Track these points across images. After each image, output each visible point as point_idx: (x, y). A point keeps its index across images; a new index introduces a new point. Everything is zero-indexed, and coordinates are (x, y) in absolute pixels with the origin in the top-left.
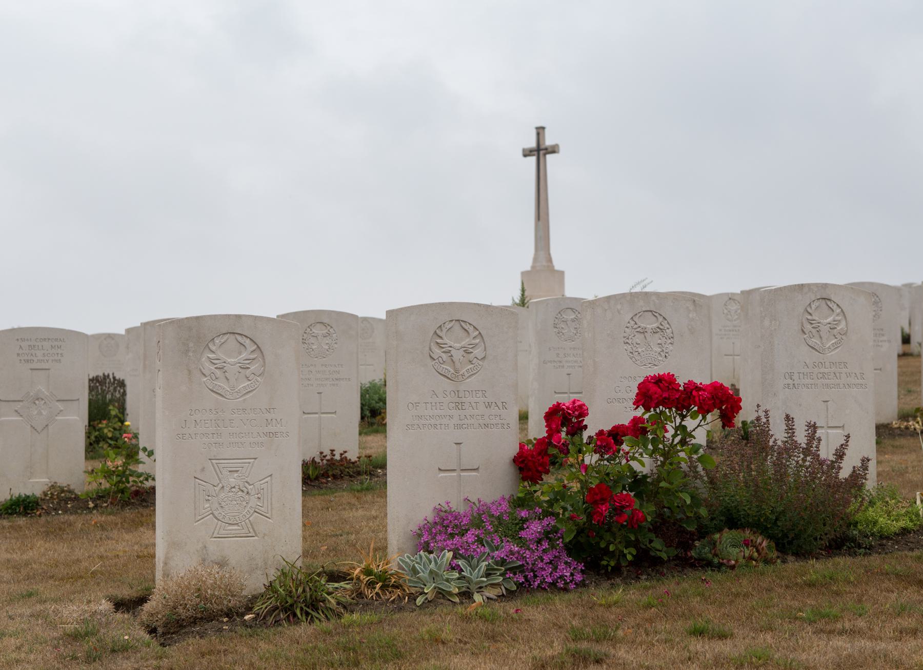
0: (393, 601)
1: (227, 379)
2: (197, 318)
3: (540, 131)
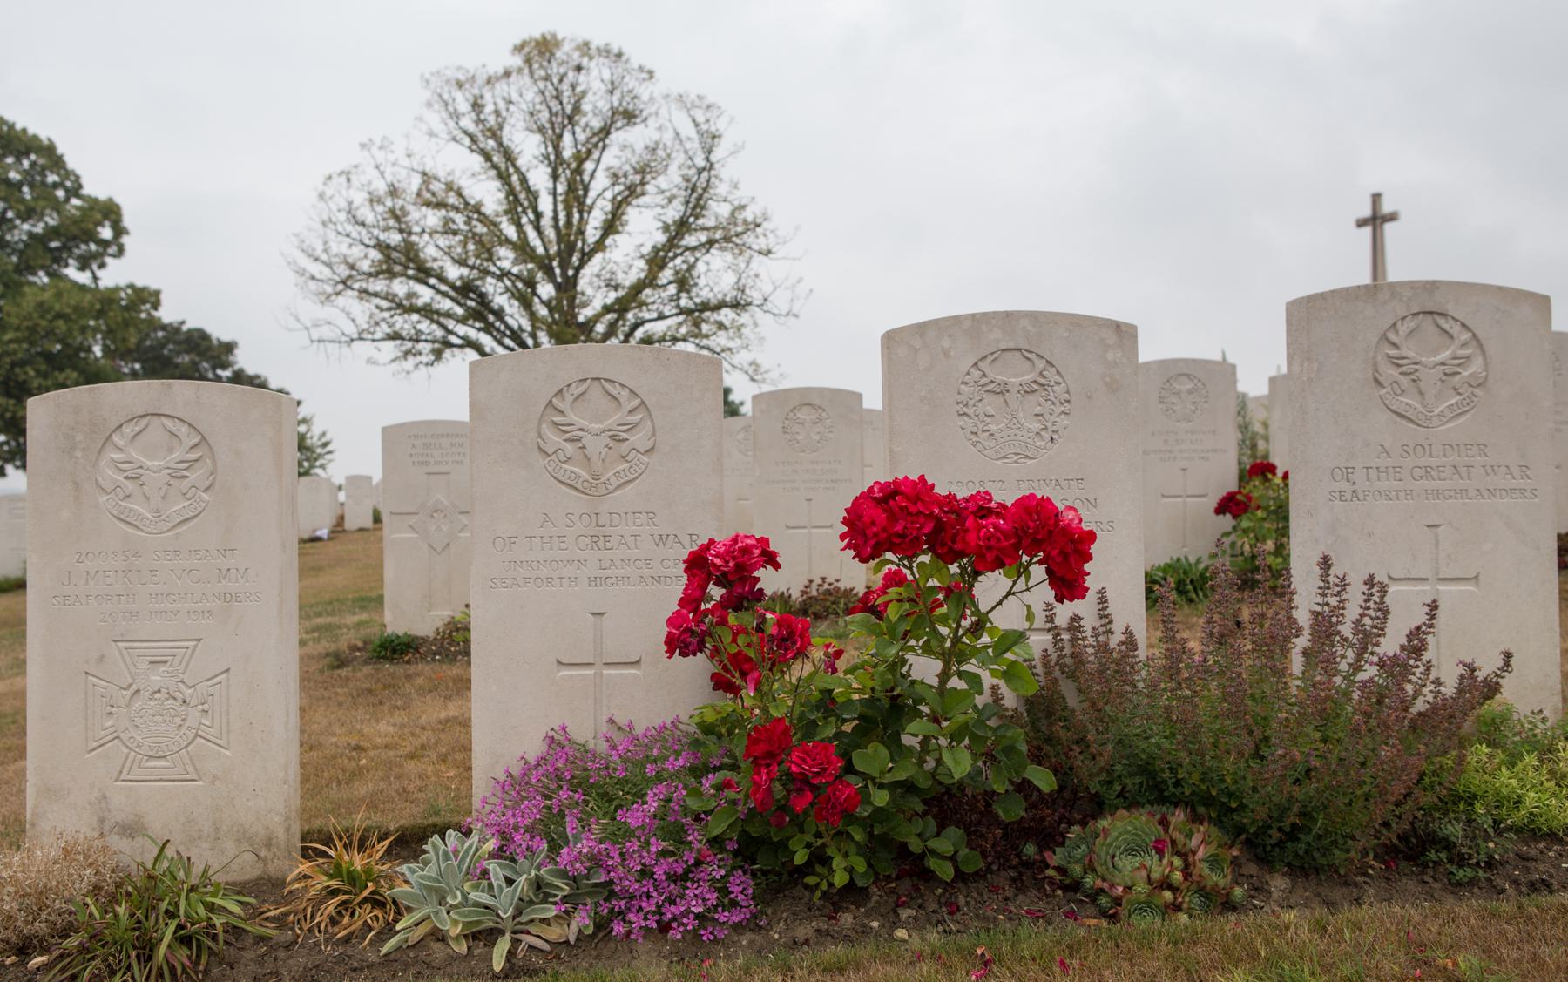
1: (148, 498)
3: (1376, 198)
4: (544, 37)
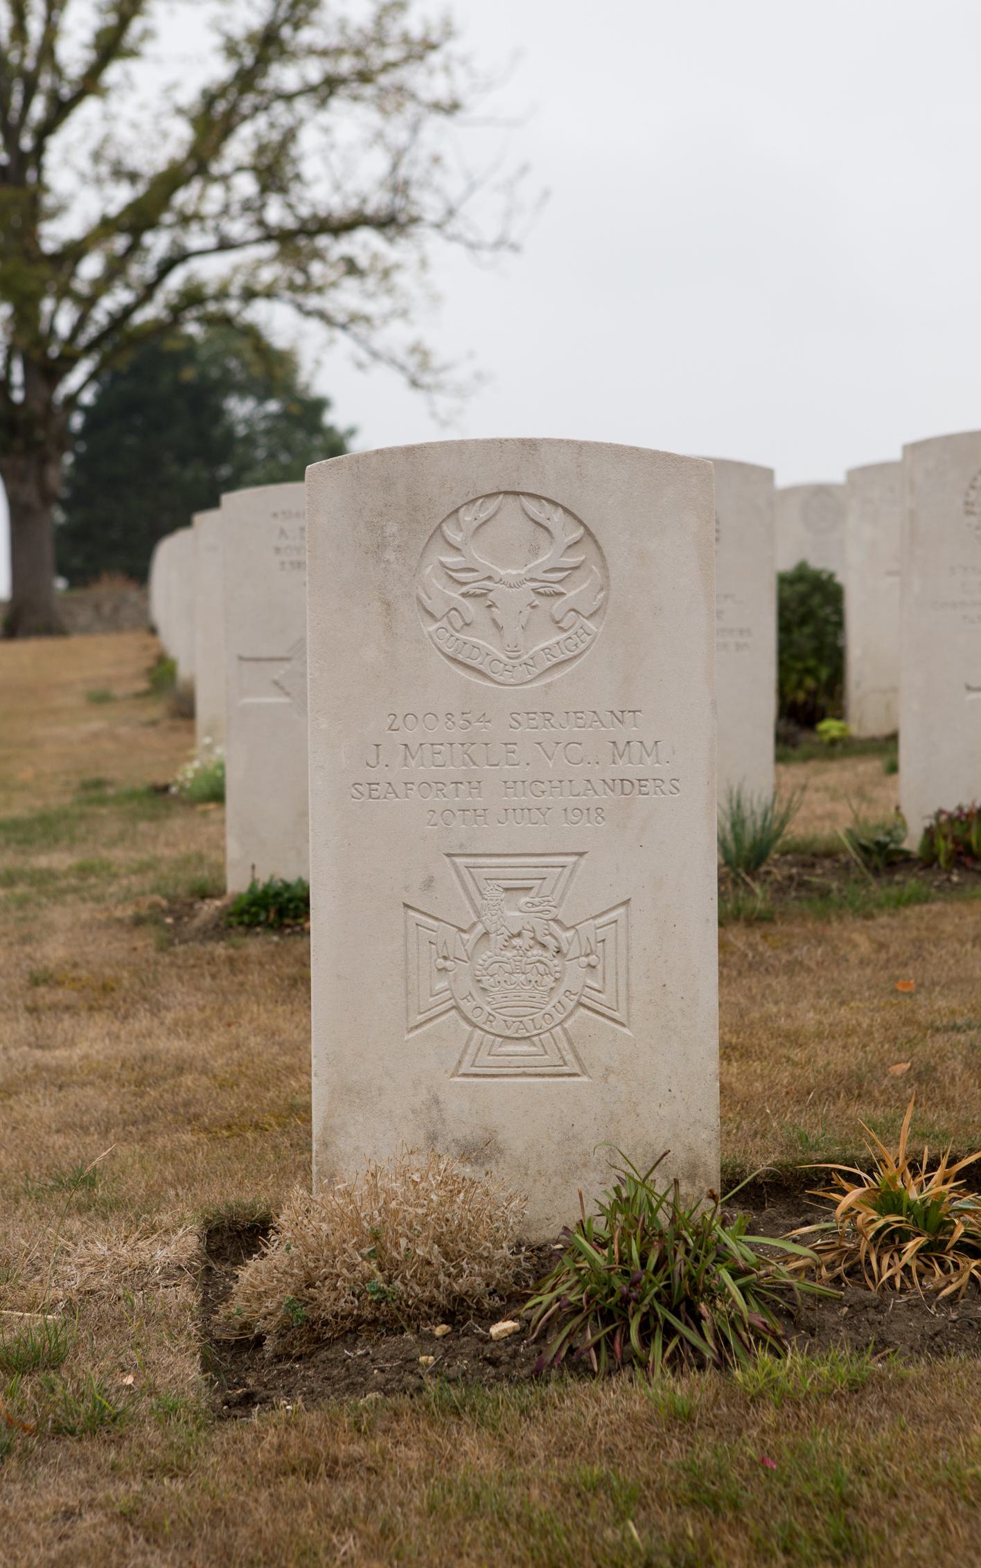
0: (952, 1300)
1: (499, 628)
2: (410, 451)
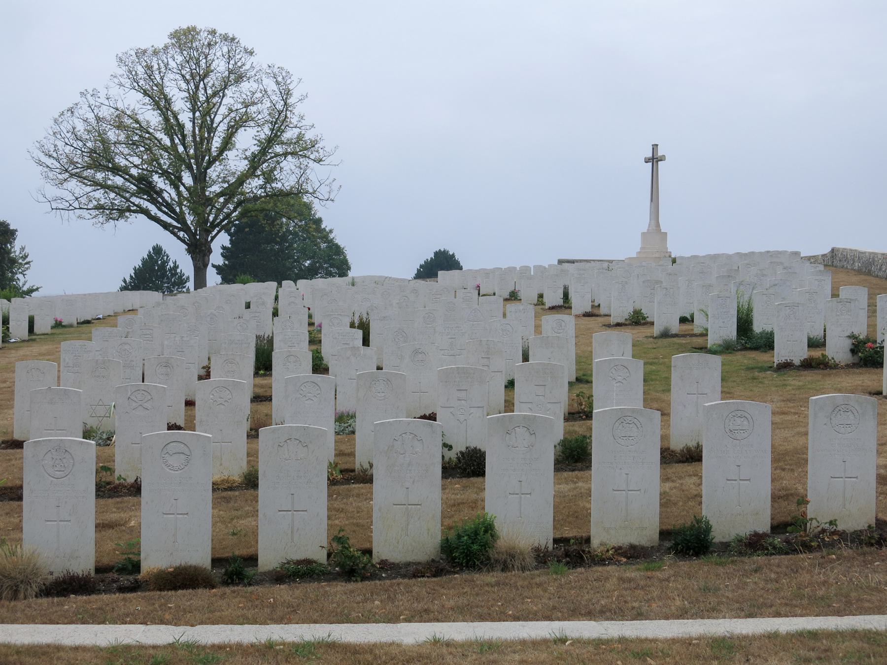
3: (655, 147)
4: (188, 28)
